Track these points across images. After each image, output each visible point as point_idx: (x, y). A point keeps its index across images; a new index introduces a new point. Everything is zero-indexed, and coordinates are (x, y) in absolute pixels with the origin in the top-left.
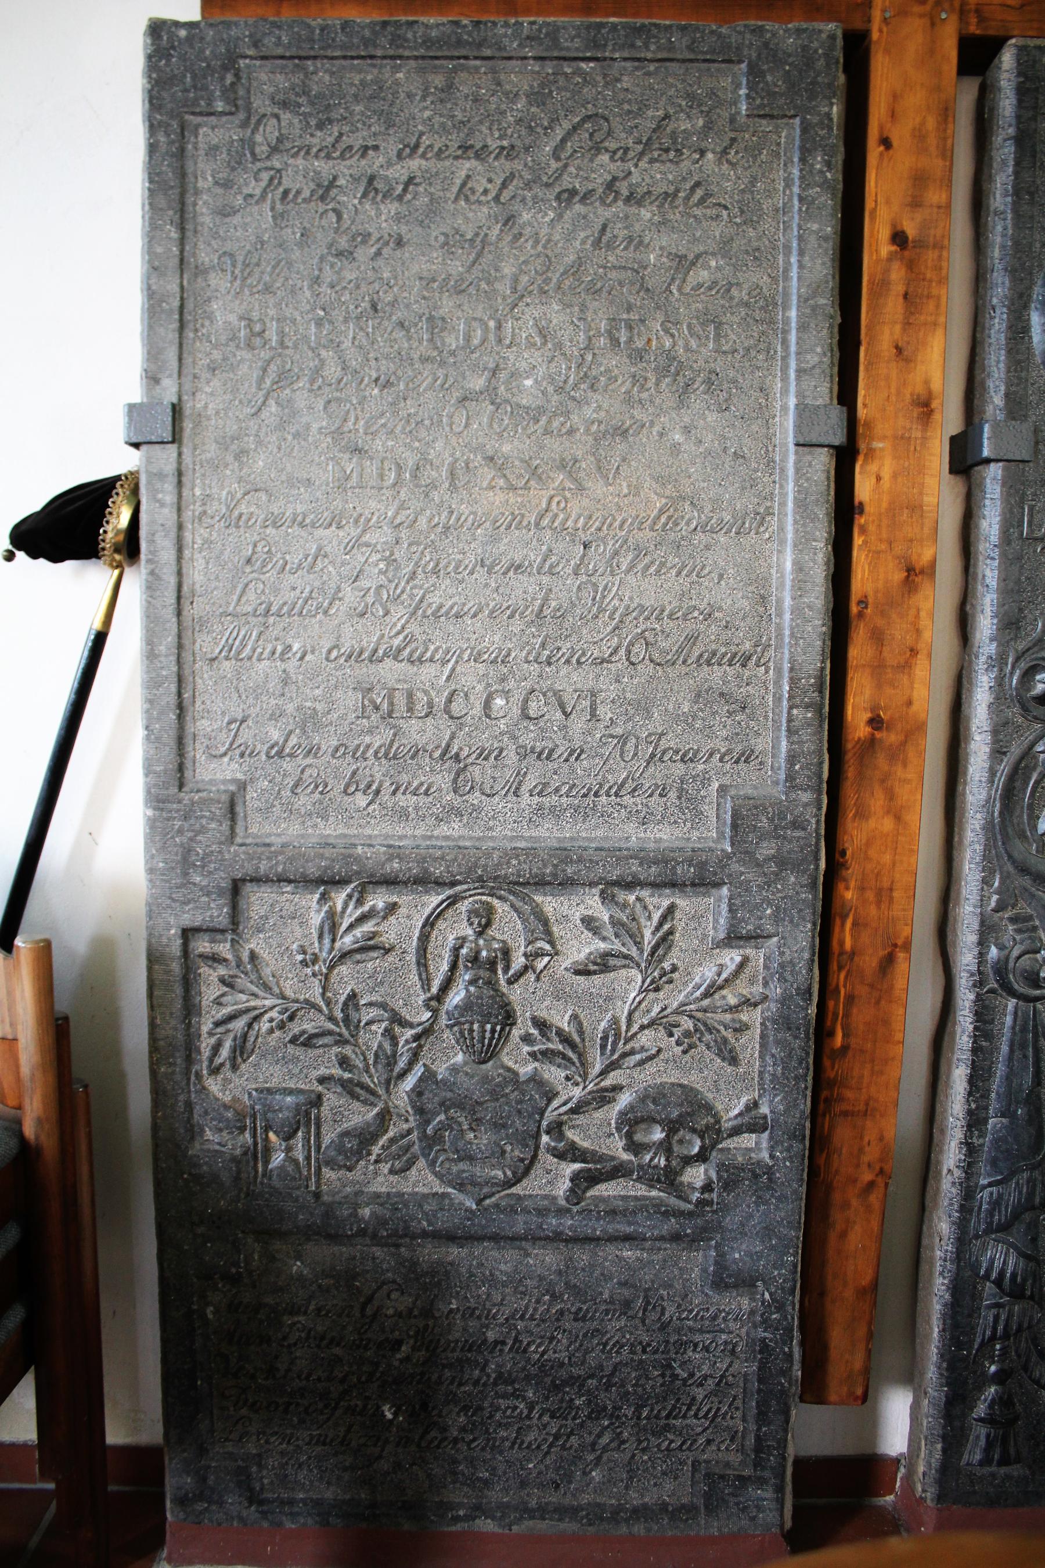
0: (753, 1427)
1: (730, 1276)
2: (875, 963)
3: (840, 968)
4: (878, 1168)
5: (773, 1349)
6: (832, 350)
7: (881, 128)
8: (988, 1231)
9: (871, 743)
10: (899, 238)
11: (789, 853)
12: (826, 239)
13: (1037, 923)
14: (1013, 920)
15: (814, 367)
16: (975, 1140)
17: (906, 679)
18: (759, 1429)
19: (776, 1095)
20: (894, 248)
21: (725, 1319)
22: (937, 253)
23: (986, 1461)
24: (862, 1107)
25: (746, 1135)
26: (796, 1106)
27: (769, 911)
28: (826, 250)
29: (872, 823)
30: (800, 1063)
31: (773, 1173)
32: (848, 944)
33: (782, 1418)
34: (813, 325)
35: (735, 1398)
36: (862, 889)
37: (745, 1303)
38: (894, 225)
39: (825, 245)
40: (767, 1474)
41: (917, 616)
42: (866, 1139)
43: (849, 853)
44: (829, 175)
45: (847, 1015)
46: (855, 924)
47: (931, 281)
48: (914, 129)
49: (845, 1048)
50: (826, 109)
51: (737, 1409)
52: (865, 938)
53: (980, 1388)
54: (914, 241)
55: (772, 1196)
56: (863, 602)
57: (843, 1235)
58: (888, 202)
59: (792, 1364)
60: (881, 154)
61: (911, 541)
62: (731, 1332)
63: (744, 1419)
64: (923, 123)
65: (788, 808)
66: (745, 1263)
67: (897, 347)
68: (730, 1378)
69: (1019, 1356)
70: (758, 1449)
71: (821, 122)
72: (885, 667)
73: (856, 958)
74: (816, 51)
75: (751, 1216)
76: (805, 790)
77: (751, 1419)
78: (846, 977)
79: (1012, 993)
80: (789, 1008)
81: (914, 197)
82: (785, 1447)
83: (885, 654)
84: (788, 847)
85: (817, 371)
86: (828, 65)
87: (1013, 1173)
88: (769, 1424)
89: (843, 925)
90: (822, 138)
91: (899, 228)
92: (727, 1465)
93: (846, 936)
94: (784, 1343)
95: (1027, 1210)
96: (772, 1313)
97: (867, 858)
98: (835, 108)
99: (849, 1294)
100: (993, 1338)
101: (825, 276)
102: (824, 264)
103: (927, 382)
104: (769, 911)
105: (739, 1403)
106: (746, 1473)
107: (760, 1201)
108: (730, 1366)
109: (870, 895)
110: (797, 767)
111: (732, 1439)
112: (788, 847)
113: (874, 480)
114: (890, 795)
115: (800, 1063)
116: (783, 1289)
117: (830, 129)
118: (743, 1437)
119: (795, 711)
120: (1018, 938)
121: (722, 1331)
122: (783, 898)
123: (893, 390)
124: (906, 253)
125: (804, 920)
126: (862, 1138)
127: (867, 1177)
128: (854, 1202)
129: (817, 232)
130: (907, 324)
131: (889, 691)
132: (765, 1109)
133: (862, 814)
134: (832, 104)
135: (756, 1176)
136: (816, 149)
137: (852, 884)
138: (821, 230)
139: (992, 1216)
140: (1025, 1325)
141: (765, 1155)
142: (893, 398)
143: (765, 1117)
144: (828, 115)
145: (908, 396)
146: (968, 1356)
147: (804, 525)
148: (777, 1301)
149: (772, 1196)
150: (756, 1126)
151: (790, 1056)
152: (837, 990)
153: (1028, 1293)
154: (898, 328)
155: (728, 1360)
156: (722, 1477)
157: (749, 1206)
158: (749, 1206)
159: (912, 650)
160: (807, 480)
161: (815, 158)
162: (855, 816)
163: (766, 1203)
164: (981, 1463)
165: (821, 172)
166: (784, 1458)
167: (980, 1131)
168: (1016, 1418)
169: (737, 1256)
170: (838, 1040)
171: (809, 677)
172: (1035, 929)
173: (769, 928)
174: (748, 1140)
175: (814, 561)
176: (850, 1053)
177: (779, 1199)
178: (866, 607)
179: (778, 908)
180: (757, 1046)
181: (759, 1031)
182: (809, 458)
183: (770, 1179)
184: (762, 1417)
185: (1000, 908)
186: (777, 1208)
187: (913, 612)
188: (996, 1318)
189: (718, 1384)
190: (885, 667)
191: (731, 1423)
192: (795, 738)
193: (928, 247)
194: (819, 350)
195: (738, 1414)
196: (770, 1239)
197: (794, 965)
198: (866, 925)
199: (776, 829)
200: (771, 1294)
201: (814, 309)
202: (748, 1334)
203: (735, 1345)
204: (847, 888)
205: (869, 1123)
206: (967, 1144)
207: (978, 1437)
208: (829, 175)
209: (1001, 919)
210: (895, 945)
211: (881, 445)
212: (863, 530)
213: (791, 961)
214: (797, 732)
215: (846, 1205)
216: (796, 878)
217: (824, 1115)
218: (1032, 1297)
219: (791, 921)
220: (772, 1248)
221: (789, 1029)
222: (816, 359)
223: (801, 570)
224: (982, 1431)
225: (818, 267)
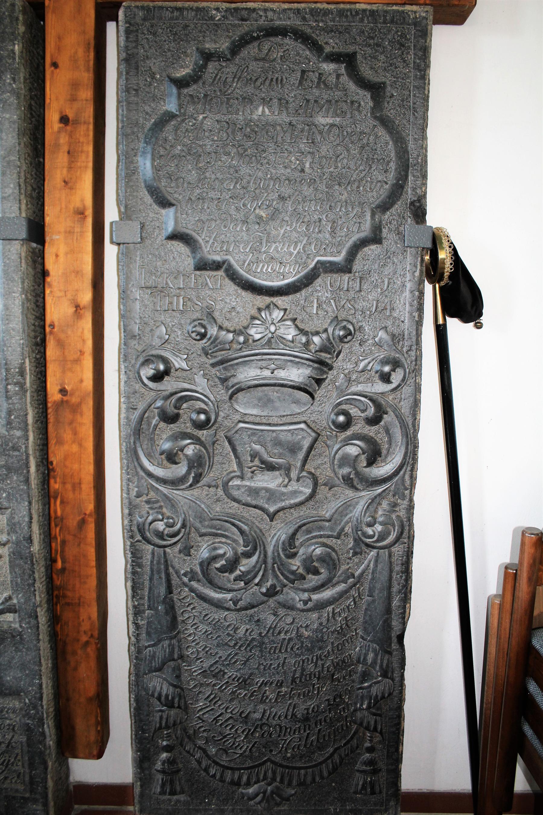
0: (27, 771)
1: (6, 689)
2: (75, 523)
3: (56, 526)
4: (90, 633)
5: (33, 729)
6: (20, 186)
7: (52, 56)
8: (151, 671)
9: (60, 404)
10: (64, 120)
11: (12, 463)
12: (14, 122)
13: (162, 504)
14: (148, 502)
15: (9, 196)
16: (139, 622)
17: (78, 368)
18: (31, 772)
19: (19, 594)
20: (62, 125)
21: (7, 712)
22: (86, 126)
23: (163, 792)
24: (77, 601)
25: (8, 614)
26: (30, 600)
27: (4, 495)
28: (14, 129)
29: (66, 447)
30: (30, 577)
31: (22, 635)
32: (59, 513)
33: (42, 766)
34: (8, 172)
35: (17, 755)
36: (64, 483)
37: (17, 704)
38: (61, 112)
39: (13, 126)
40: (38, 796)
41: (82, 333)
42: (81, 619)
43: (54, 463)
44: (14, 85)
45: (63, 551)
46: (62, 502)
47: (83, 143)
48: (71, 56)
49: (63, 569)
50: (11, 47)
51: (19, 760)
52: (68, 509)
53: (157, 754)
54: (73, 121)
55: (24, 647)
56: (52, 325)
57: (76, 669)
58: (57, 99)
59: (45, 738)
60: (52, 72)
61: (77, 290)
62: (11, 719)
63: (23, 767)
64: (76, 52)
65: (9, 439)
66: (13, 683)
67: (65, 182)
68: (13, 744)
69: (177, 738)
70: (32, 782)
71: (9, 56)
72: (67, 361)
73: (64, 521)
74: (4, 13)
75: (13, 658)
76: (18, 430)
77: (26, 766)
78: (60, 530)
79: (149, 542)
80: (20, 547)
81: (72, 95)
82: (46, 782)
83: (66, 353)
84: (11, 460)
85: (12, 198)
86: (11, 21)
87: (160, 641)
88: (36, 770)
89: (55, 503)
90: (10, 65)
91: (64, 114)
92: (17, 791)
93: (58, 508)
94: (39, 727)
95: (170, 661)
96: (30, 711)
97: (65, 466)
98: (16, 47)
99: (82, 700)
100: (160, 728)
101: (14, 143)
102: (13, 137)
103: (82, 201)
104: (4, 495)
105: (19, 757)
106: (27, 795)
107: (17, 650)
108: (13, 736)
109: (69, 486)
110: (13, 417)
111: (18, 777)
112: (11, 460)
113: (54, 257)
114: (75, 433)
115: (30, 577)
116: (35, 697)
117: (14, 59)
118: (24, 776)
119: (9, 387)
120: (151, 512)
121: (6, 718)
122: (11, 488)
123: (63, 206)
124: (68, 128)
125: (23, 500)
126: (79, 618)
127: (84, 638)
128: (79, 652)
129: (8, 119)
130: (70, 168)
131: (69, 374)
132: (15, 601)
133: (60, 442)
134: (14, 44)
135: (13, 637)
136: (7, 71)
137: (58, 480)
138: (11, 117)
139: (152, 663)
140: (178, 721)
141: (17, 626)
142: (64, 210)
143: (15, 605)
144: (13, 51)
145: (72, 209)
146: (149, 736)
147: (8, 284)
148: (32, 704)
149: (24, 647)
150: (12, 610)
151: (24, 573)
152: (56, 538)
153: (176, 705)
154: (65, 171)
155: (11, 734)
156: (14, 798)
157: (11, 652)
158: (11, 652)
159: (81, 351)
160: (9, 259)
161: (6, 77)
162: (56, 444)
163: (20, 651)
164: (160, 794)
165: (10, 84)
166: (46, 788)
167: (142, 617)
168: (178, 771)
169: (8, 678)
170: (59, 564)
171: (16, 368)
172: (161, 507)
173: (5, 504)
174: (9, 617)
175: (14, 304)
176: (67, 572)
177: (27, 649)
178: (54, 328)
179: (9, 493)
180: (8, 567)
181: (8, 559)
182: (9, 247)
183: (21, 638)
184: (31, 765)
185: (138, 496)
186: (27, 654)
187: (80, 330)
188: (161, 718)
189: (8, 747)
190: (67, 361)
191: (17, 768)
192: (10, 401)
193: (81, 123)
194: (12, 186)
195: (20, 763)
196: (25, 671)
197: (20, 525)
198: (68, 503)
199: (4, 451)
200: (29, 700)
201: (9, 162)
202: (20, 720)
203: (14, 726)
204: (56, 482)
205: (82, 610)
206: (136, 624)
207: (158, 780)
208: (14, 85)
209: (141, 501)
210: (85, 514)
211: (57, 237)
212: (50, 286)
213: (19, 522)
214: (11, 398)
215: (74, 653)
216: (17, 477)
217: (57, 605)
218: (179, 707)
219: (17, 501)
220: (27, 675)
221: (22, 558)
222: (11, 191)
223: (7, 309)
224: (160, 777)
225: (10, 139)
